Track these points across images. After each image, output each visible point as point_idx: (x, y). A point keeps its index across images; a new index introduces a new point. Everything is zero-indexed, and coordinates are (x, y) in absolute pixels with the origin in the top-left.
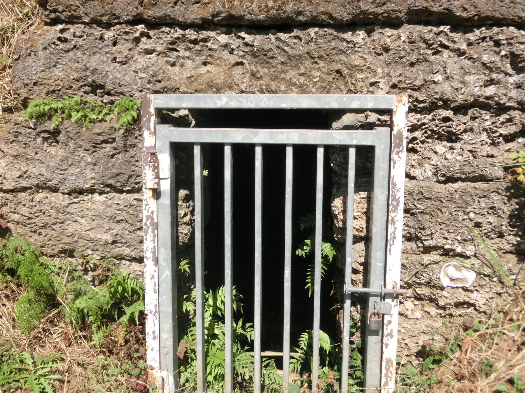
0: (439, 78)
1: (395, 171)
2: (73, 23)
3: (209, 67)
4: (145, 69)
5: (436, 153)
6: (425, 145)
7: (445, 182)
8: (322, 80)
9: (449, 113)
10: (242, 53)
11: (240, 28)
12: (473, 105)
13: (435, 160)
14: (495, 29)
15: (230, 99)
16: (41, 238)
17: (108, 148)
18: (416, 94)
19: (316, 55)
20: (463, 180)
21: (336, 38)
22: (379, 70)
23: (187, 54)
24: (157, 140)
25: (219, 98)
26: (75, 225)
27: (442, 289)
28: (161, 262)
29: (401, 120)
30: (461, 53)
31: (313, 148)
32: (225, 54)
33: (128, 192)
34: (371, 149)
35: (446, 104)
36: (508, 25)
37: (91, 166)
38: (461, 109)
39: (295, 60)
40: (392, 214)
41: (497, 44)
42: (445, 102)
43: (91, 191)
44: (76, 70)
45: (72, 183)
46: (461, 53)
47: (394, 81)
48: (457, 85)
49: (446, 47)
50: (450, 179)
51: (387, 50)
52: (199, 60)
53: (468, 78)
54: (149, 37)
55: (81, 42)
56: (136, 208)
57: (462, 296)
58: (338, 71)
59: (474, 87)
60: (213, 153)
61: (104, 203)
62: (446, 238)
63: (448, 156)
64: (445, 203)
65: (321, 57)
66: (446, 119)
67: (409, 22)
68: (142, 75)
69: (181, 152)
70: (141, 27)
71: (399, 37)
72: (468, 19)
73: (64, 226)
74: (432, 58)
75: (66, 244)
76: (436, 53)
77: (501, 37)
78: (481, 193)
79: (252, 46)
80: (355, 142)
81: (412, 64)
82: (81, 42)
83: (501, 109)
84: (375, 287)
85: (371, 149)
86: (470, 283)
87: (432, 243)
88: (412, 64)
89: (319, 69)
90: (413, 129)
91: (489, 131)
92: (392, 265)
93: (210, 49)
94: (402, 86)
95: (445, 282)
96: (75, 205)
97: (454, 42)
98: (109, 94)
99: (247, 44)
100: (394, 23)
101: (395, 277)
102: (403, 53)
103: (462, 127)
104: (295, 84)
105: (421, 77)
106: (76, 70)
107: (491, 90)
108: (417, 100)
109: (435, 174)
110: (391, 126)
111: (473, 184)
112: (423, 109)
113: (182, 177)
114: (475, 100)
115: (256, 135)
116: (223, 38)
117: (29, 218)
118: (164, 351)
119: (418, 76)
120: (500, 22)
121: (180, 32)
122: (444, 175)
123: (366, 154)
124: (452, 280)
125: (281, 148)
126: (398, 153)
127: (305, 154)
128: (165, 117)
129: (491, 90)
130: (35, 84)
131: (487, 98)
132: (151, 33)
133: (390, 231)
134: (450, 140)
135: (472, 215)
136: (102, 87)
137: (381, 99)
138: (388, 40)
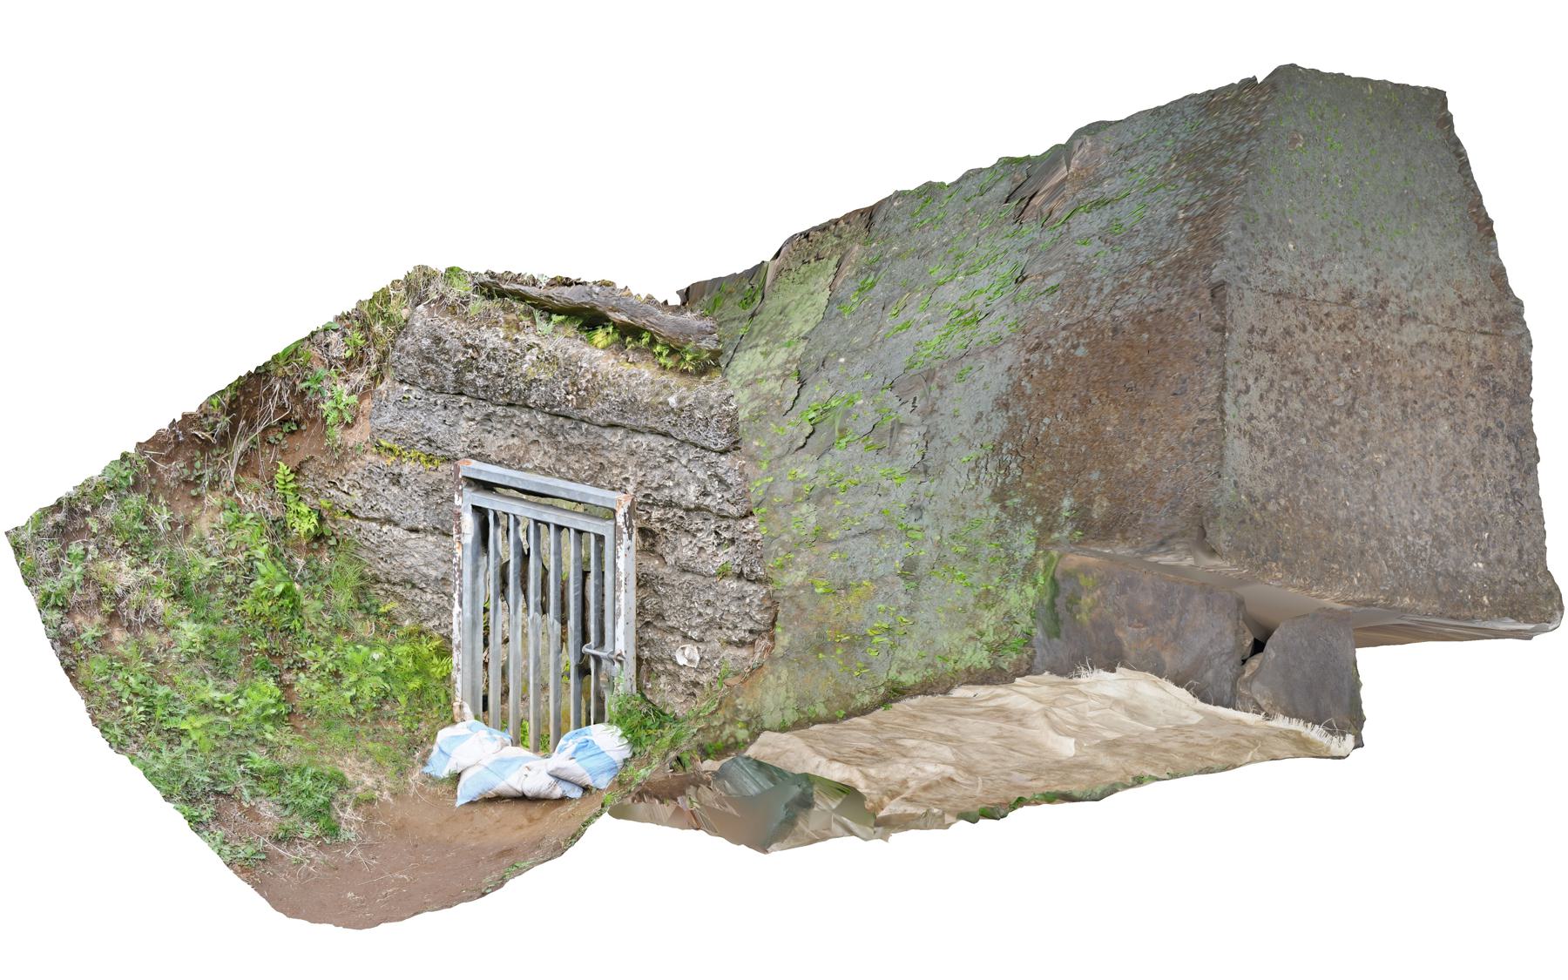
3: (516, 440)
50: (685, 571)
52: (509, 432)
70: (464, 399)
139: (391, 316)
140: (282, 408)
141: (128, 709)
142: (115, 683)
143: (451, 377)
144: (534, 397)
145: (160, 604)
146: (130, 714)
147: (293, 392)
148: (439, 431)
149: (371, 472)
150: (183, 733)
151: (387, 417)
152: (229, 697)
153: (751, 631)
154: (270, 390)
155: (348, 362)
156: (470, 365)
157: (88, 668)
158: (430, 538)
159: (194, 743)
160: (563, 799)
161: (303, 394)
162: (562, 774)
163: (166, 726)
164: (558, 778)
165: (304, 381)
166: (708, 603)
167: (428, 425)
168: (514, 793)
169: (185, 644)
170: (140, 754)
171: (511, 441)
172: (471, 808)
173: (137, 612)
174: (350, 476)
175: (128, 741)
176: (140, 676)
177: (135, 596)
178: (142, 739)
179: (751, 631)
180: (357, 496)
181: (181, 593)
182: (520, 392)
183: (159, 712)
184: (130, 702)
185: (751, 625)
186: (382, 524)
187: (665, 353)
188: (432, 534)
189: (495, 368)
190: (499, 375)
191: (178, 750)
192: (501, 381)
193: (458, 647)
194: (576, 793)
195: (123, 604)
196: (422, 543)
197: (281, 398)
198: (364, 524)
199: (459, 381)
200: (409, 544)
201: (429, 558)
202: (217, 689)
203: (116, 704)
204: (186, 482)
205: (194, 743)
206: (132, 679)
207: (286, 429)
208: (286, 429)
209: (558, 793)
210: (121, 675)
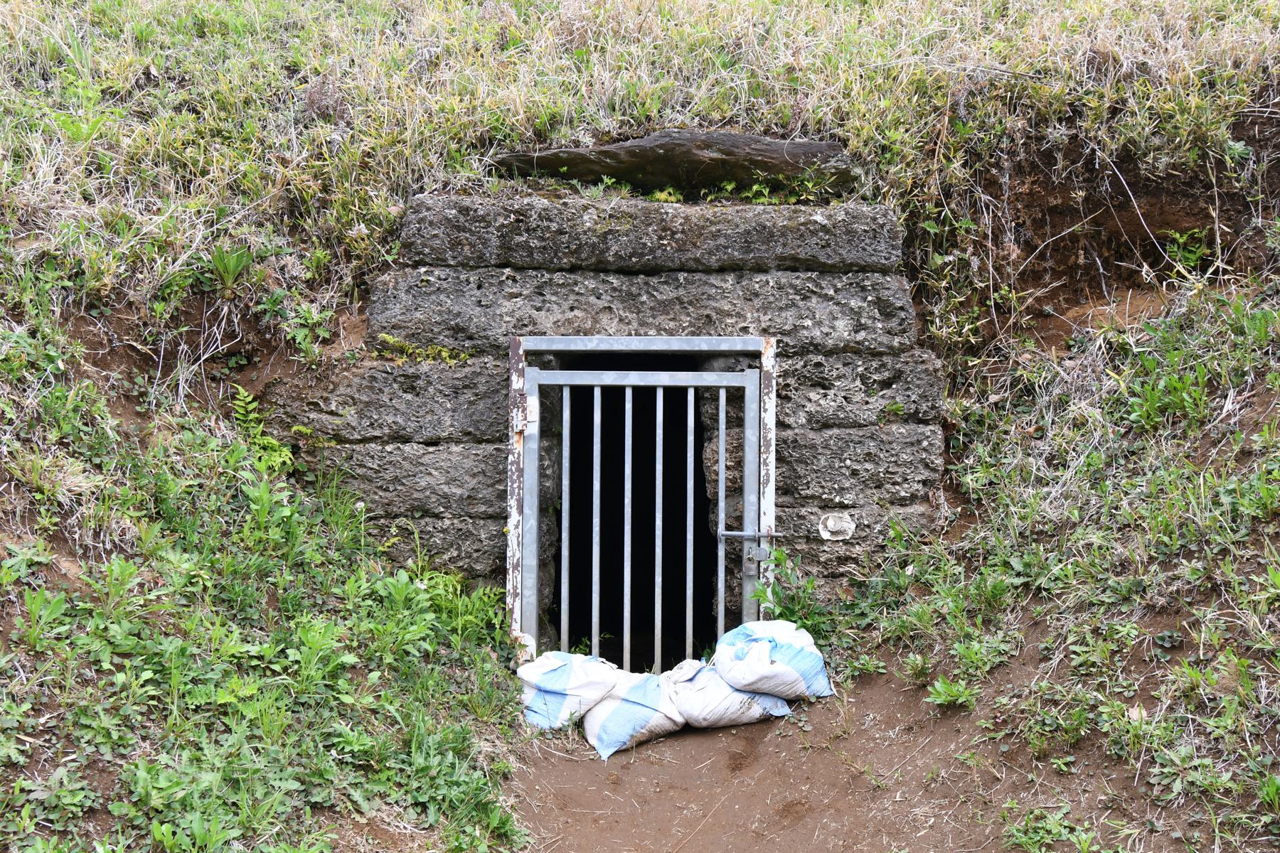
0: (808, 323)
1: (763, 413)
2: (437, 266)
3: (576, 312)
4: (511, 314)
5: (810, 400)
6: (800, 392)
7: (820, 430)
8: (691, 324)
9: (820, 358)
10: (609, 298)
11: (606, 271)
12: (846, 349)
13: (810, 407)
14: (861, 275)
15: (601, 341)
16: (388, 494)
17: (469, 395)
18: (786, 339)
19: (686, 300)
20: (839, 426)
21: (706, 283)
22: (749, 315)
23: (554, 298)
24: (527, 381)
25: (590, 341)
26: (428, 478)
27: (822, 542)
28: (526, 510)
29: (768, 361)
30: (827, 298)
31: (684, 390)
32: (592, 299)
33: (488, 441)
34: (741, 390)
35: (817, 348)
36: (873, 271)
37: (450, 413)
38: (829, 353)
39: (664, 307)
40: (764, 456)
41: (863, 289)
42: (816, 346)
43: (449, 440)
44: (440, 313)
45: (428, 433)
46: (827, 298)
47: (764, 325)
48: (826, 330)
49: (814, 293)
50: (826, 426)
51: (757, 295)
52: (566, 305)
53: (837, 323)
54: (515, 280)
55: (445, 285)
56: (501, 457)
57: (842, 550)
58: (708, 316)
59: (843, 329)
60: (582, 395)
61: (460, 454)
62: (823, 487)
63: (822, 402)
64: (820, 451)
65: (690, 303)
66: (819, 365)
67: (779, 268)
68: (508, 319)
69: (549, 395)
70: (507, 271)
71: (768, 283)
72: (833, 266)
73: (91, 799)
74: (801, 304)
75: (415, 499)
76: (805, 298)
77: (867, 283)
78: (857, 439)
79: (620, 291)
80: (725, 384)
81: (781, 309)
82: (445, 285)
83: (876, 354)
84: (749, 530)
85: (741, 390)
86: (850, 534)
87: (809, 492)
88: (781, 309)
89: (688, 315)
90: (785, 374)
91: (864, 379)
92: (763, 510)
93: (578, 294)
94: (772, 330)
95: (825, 535)
96: (431, 456)
97: (822, 288)
98: (471, 338)
99: (615, 289)
100: (761, 269)
101: (769, 522)
102: (772, 299)
103: (835, 373)
104: (665, 330)
105: (791, 321)
106: (440, 313)
107: (861, 336)
108: (787, 344)
109: (809, 421)
110: (760, 368)
111: (848, 431)
112: (795, 354)
113: (549, 428)
114: (845, 346)
115: (627, 376)
116: (591, 284)
117: (377, 472)
118: (527, 614)
119: (788, 319)
120: (863, 269)
121: (547, 276)
122: (818, 422)
123: (736, 396)
124: (833, 533)
125: (651, 390)
126: (767, 394)
127: (675, 396)
128: (537, 359)
129: (861, 336)
130: (393, 327)
131: (857, 343)
132: (518, 277)
133: (763, 473)
134: (824, 387)
135: (848, 462)
136: (463, 330)
137: (752, 342)
138: (757, 286)
139: (375, 216)
140: (230, 335)
141: (120, 678)
142: (82, 639)
143: (495, 241)
144: (614, 248)
145: (126, 522)
146: (124, 688)
147: (244, 316)
148: (475, 317)
149: (373, 378)
150: (224, 710)
151: (397, 309)
152: (268, 649)
153: (924, 483)
154: (216, 314)
155: (310, 284)
156: (515, 228)
157: (26, 615)
158: (454, 448)
159: (252, 724)
160: (767, 720)
161: (258, 316)
162: (765, 686)
163: (192, 702)
164: (753, 692)
165: (258, 303)
166: (869, 457)
167: (456, 309)
168: (669, 726)
169: (179, 581)
170: (164, 758)
171: (570, 315)
172: (623, 759)
173: (96, 535)
174: (342, 390)
175: (132, 738)
176: (126, 624)
177: (88, 509)
178: (155, 731)
179: (924, 483)
180: (350, 414)
181: (157, 509)
182: (594, 246)
183: (176, 678)
184: (121, 668)
185: (926, 474)
186: (385, 443)
187: (766, 192)
188: (458, 442)
189: (554, 226)
190: (561, 232)
191: (229, 741)
192: (565, 238)
193: (515, 567)
194: (782, 710)
195: (72, 520)
196: (445, 456)
197: (230, 321)
198: (357, 447)
199: (506, 247)
200: (425, 460)
201: (453, 473)
202: (245, 640)
203: (89, 674)
204: (127, 397)
205: (252, 724)
206: (114, 629)
207: (232, 363)
208: (232, 363)
209: (756, 711)
210: (91, 625)
